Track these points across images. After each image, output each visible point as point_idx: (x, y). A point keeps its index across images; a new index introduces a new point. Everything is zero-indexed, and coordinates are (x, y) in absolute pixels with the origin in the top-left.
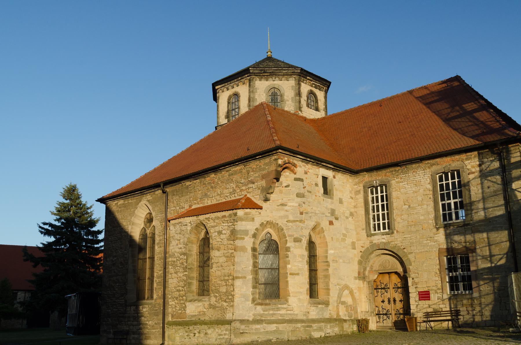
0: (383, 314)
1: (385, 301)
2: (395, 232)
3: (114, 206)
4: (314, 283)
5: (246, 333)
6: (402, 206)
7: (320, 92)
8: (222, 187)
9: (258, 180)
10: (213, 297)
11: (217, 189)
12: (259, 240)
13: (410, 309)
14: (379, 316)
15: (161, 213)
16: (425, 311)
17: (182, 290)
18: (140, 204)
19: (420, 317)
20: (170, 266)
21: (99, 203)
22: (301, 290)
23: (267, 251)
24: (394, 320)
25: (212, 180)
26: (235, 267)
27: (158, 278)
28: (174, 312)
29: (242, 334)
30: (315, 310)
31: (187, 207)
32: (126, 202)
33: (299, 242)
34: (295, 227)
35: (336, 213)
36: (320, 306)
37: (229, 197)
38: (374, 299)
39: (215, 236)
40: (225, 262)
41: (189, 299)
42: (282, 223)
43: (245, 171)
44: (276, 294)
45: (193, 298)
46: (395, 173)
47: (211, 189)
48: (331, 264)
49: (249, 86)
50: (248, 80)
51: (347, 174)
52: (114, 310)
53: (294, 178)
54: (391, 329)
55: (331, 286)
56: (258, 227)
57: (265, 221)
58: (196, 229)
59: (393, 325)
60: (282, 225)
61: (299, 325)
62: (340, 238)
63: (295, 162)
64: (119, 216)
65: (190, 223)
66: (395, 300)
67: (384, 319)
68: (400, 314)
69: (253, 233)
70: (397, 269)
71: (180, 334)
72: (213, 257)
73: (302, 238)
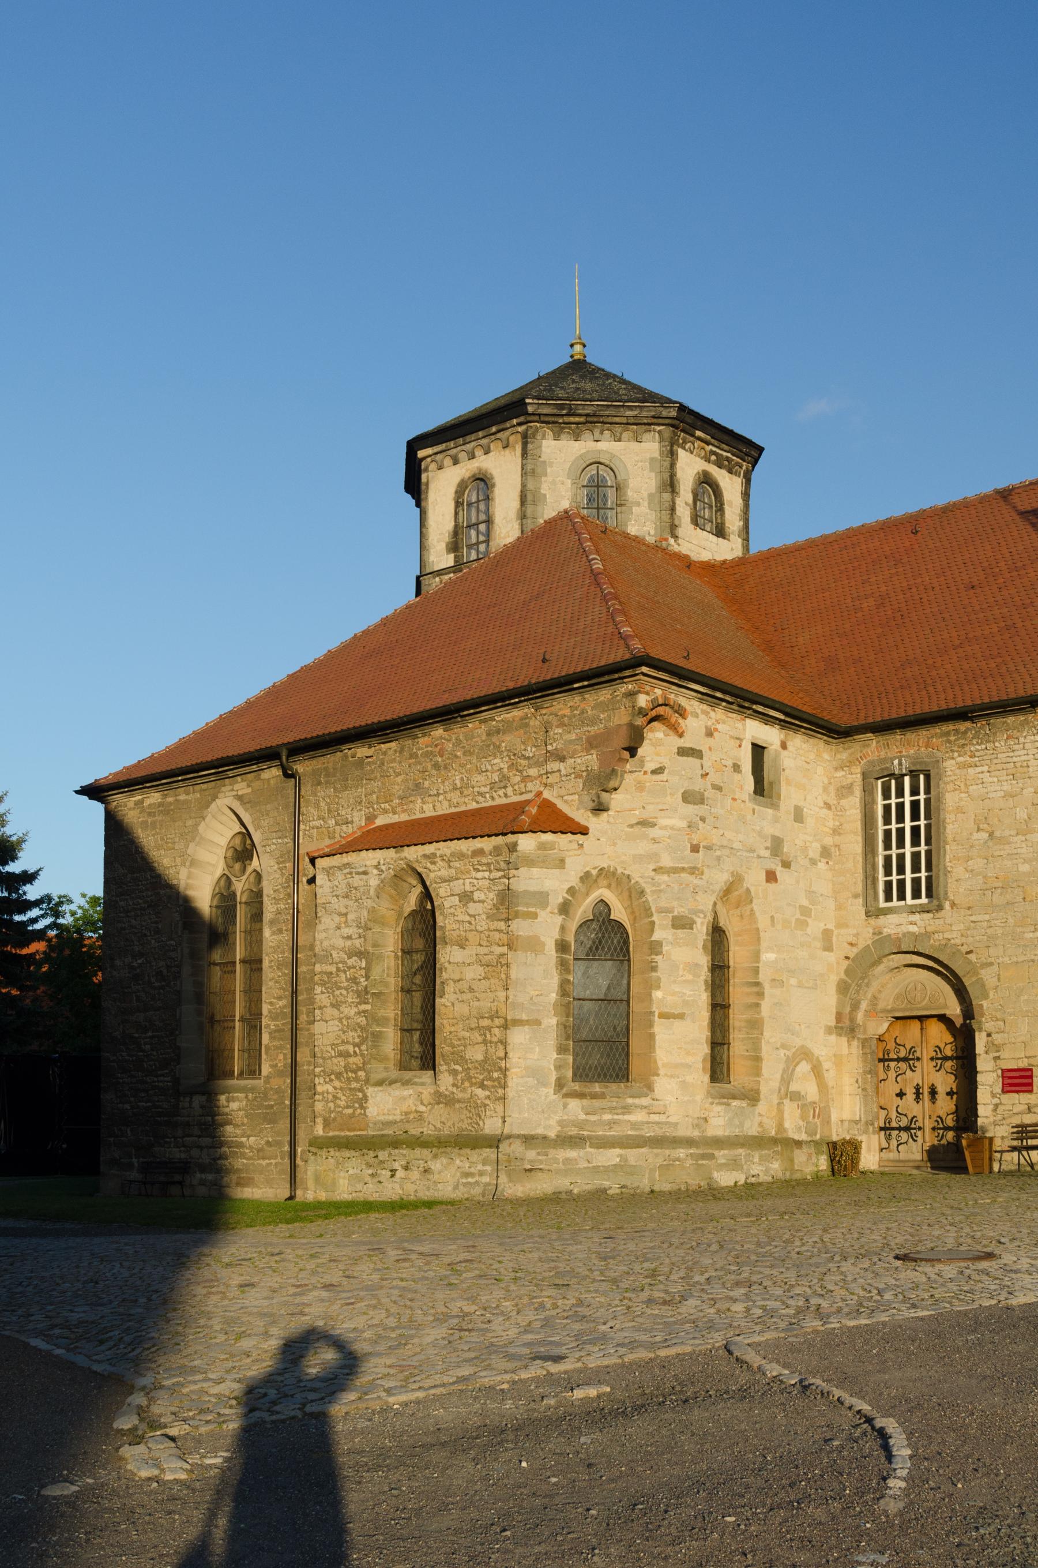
0: (900, 1129)
1: (905, 1094)
2: (947, 905)
3: (130, 809)
4: (720, 1041)
5: (541, 1169)
6: (971, 834)
7: (731, 479)
8: (468, 766)
9: (575, 752)
10: (446, 1074)
11: (453, 772)
12: (578, 917)
13: (977, 1116)
14: (888, 1132)
15: (280, 834)
16: (1016, 1121)
17: (355, 1052)
18: (213, 806)
19: (1003, 1138)
20: (316, 987)
21: (86, 798)
22: (689, 1060)
23: (594, 952)
24: (928, 1144)
25: (436, 746)
26: (511, 993)
27: (274, 1017)
28: (331, 1112)
29: (528, 1174)
30: (722, 1114)
31: (359, 819)
32: (170, 799)
33: (686, 928)
34: (676, 887)
35: (785, 850)
36: (735, 1103)
37: (488, 795)
38: (877, 1088)
39: (451, 907)
40: (480, 980)
41: (375, 1077)
42: (640, 874)
43: (537, 723)
44: (620, 1069)
45: (384, 1075)
46: (955, 741)
47: (434, 772)
48: (768, 990)
49: (523, 456)
50: (519, 436)
51: (820, 736)
52: (141, 1104)
53: (678, 748)
54: (918, 1168)
55: (765, 1050)
56: (574, 884)
57: (595, 868)
58: (396, 885)
59: (926, 1158)
60: (641, 881)
61: (681, 1153)
62: (793, 920)
63: (683, 702)
64: (148, 840)
65: (377, 867)
66: (933, 1092)
67: (902, 1141)
68: (947, 1129)
69: (561, 900)
70: (946, 1006)
71: (351, 1172)
72: (446, 965)
73: (694, 917)
